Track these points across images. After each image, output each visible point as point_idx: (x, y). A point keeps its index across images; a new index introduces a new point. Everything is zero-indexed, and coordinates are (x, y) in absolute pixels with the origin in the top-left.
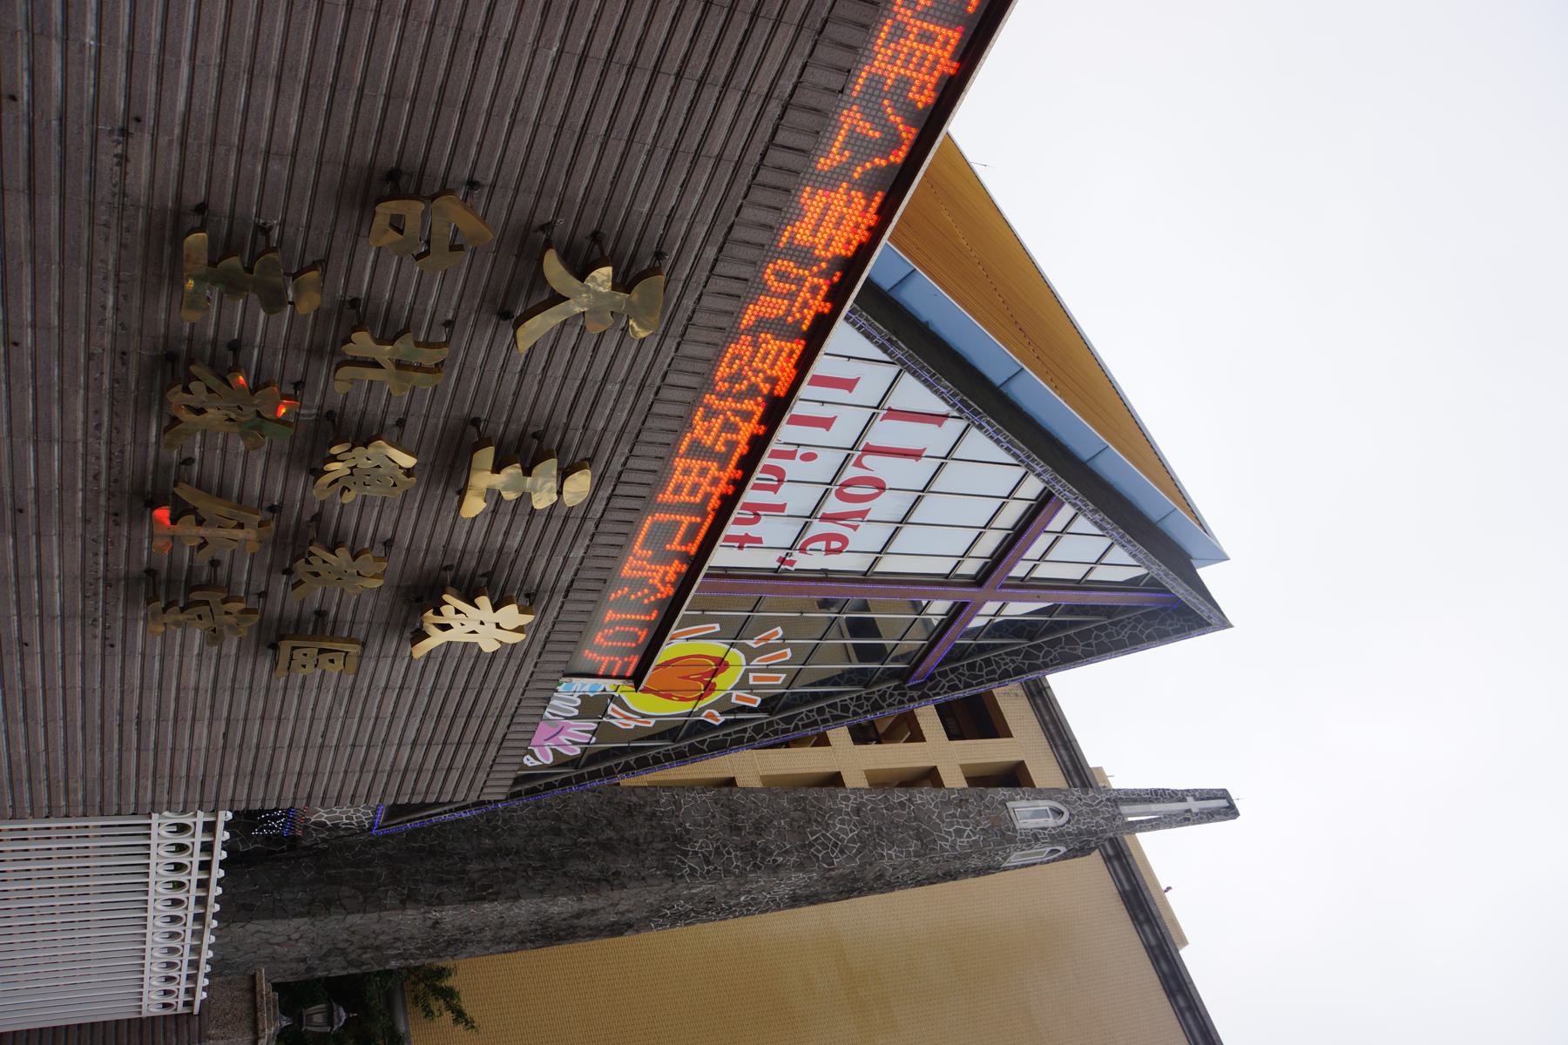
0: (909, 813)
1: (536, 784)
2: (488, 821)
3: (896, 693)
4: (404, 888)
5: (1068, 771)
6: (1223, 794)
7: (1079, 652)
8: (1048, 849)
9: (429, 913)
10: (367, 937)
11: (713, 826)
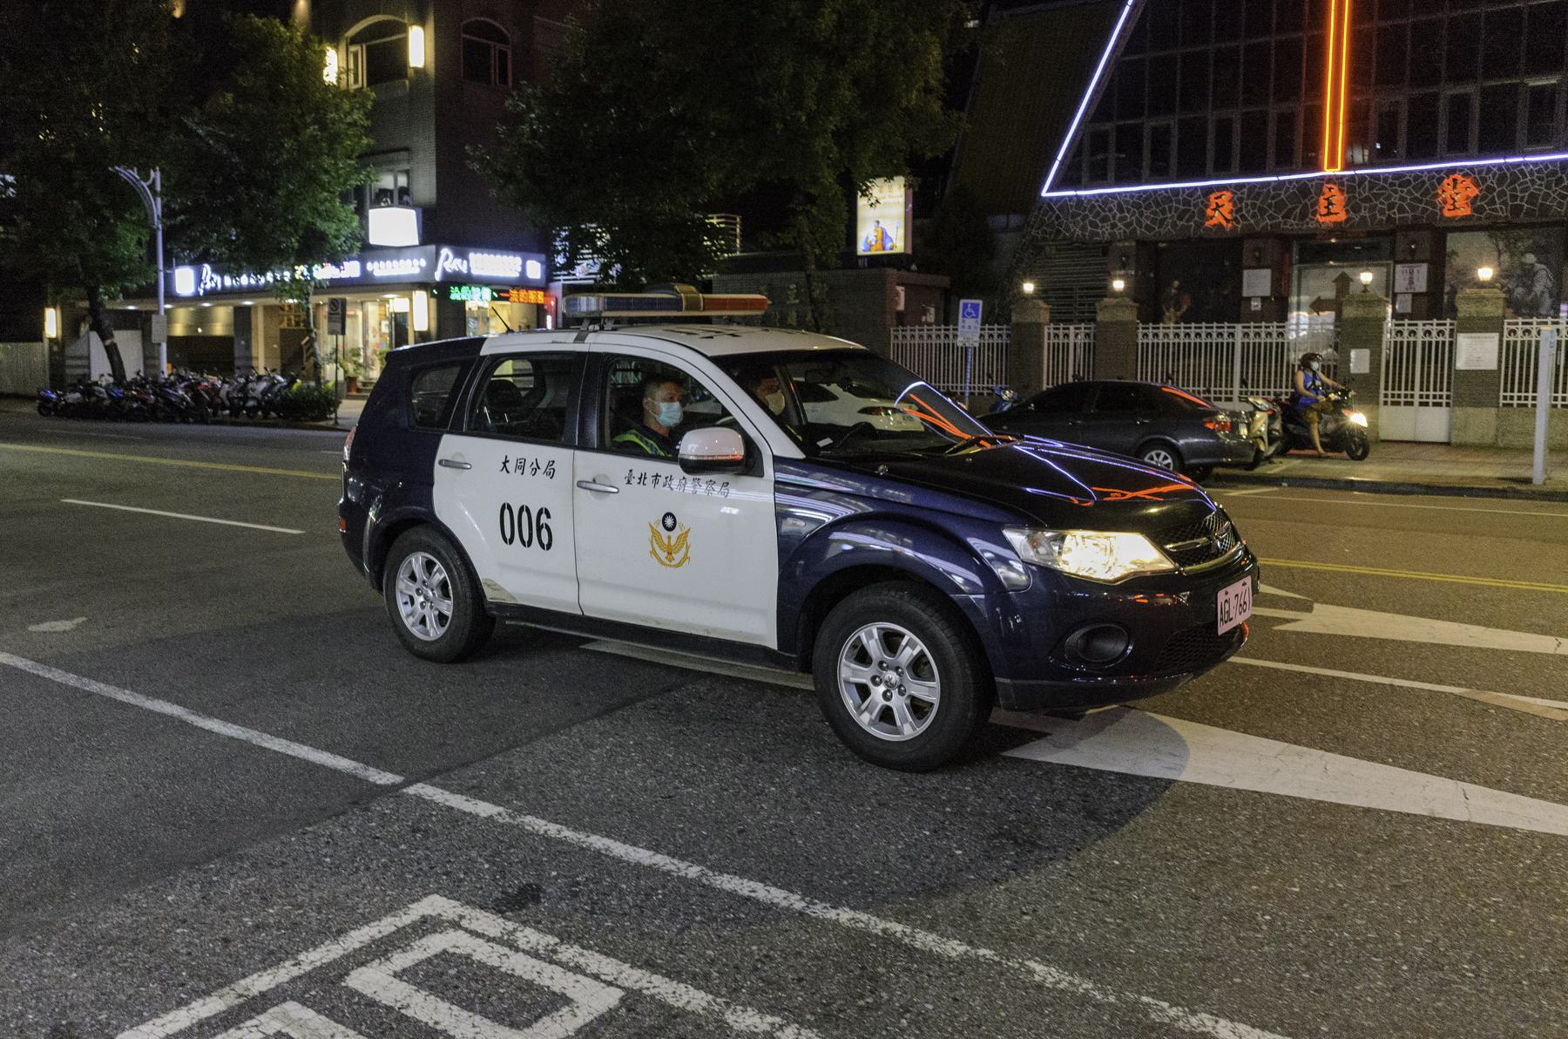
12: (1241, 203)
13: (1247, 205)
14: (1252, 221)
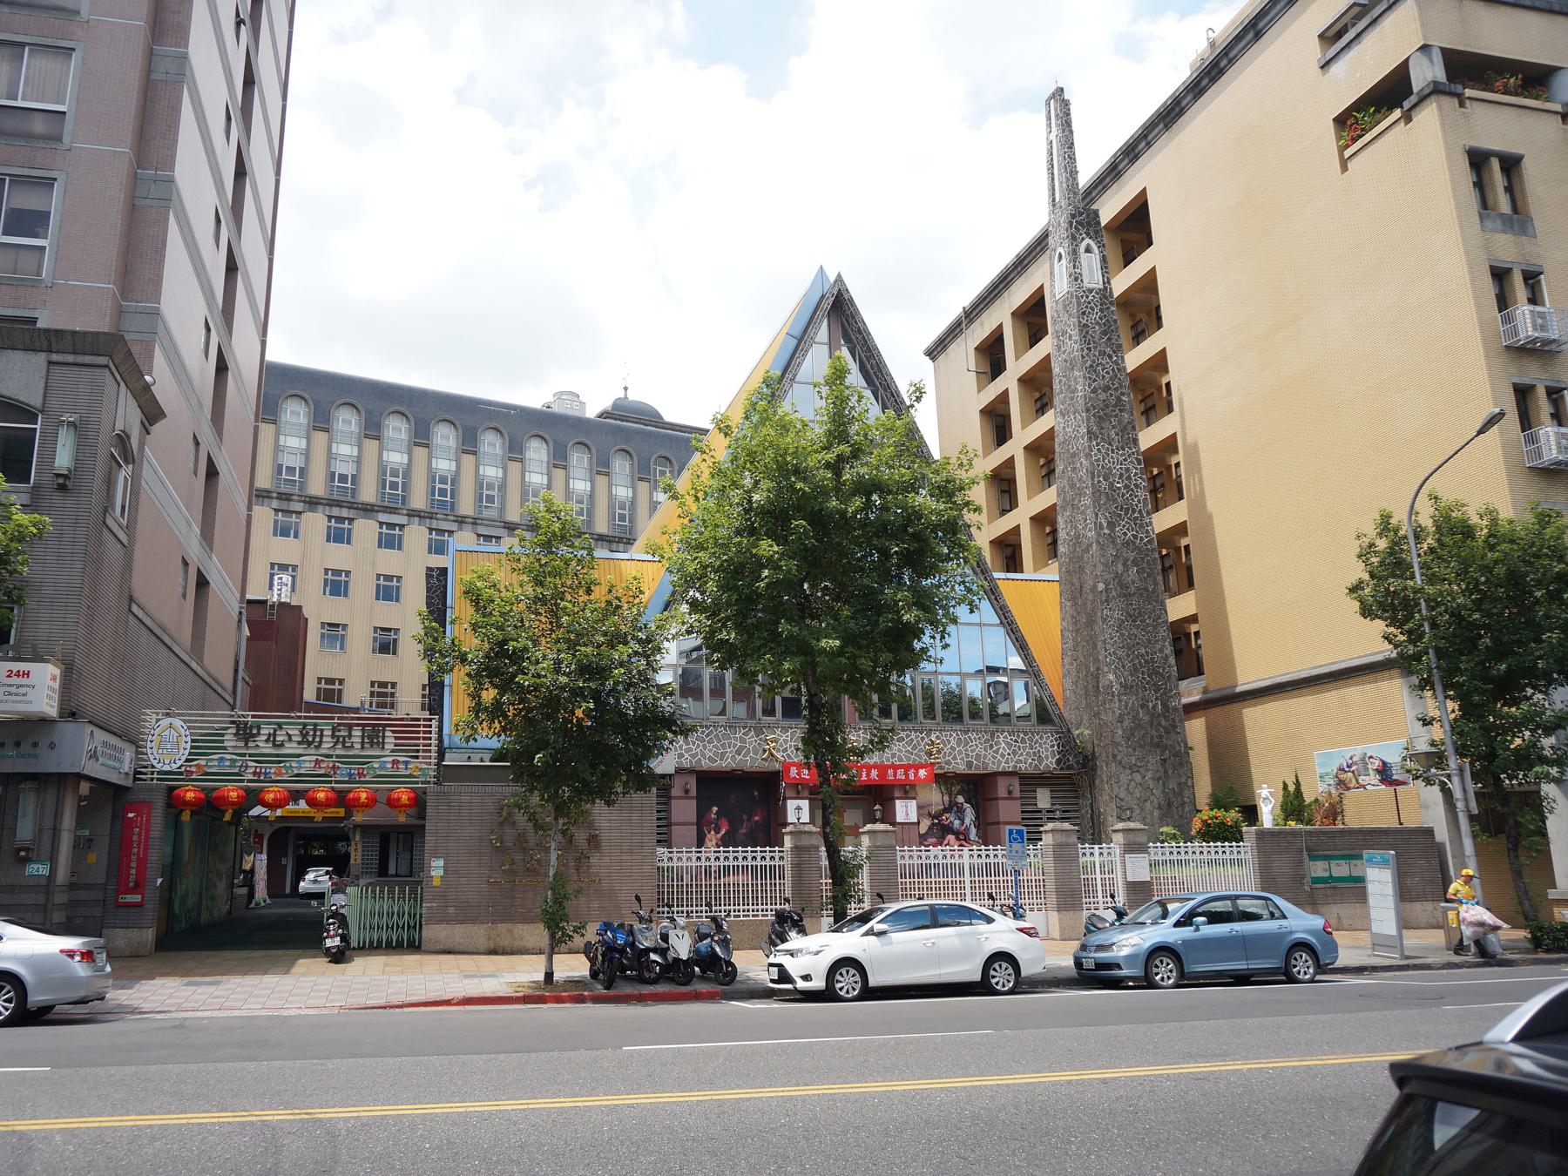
13: (791, 746)
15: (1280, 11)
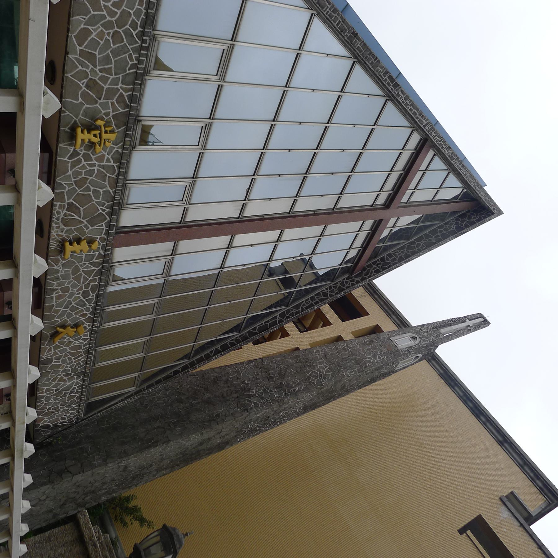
0: (349, 353)
1: (168, 373)
2: (141, 404)
3: (348, 281)
4: (103, 452)
5: (398, 325)
6: (480, 316)
7: (434, 240)
8: (414, 357)
9: (121, 462)
10: (86, 487)
11: (259, 379)
12: (96, 159)
13: (94, 165)
14: (70, 173)
15: (517, 461)
